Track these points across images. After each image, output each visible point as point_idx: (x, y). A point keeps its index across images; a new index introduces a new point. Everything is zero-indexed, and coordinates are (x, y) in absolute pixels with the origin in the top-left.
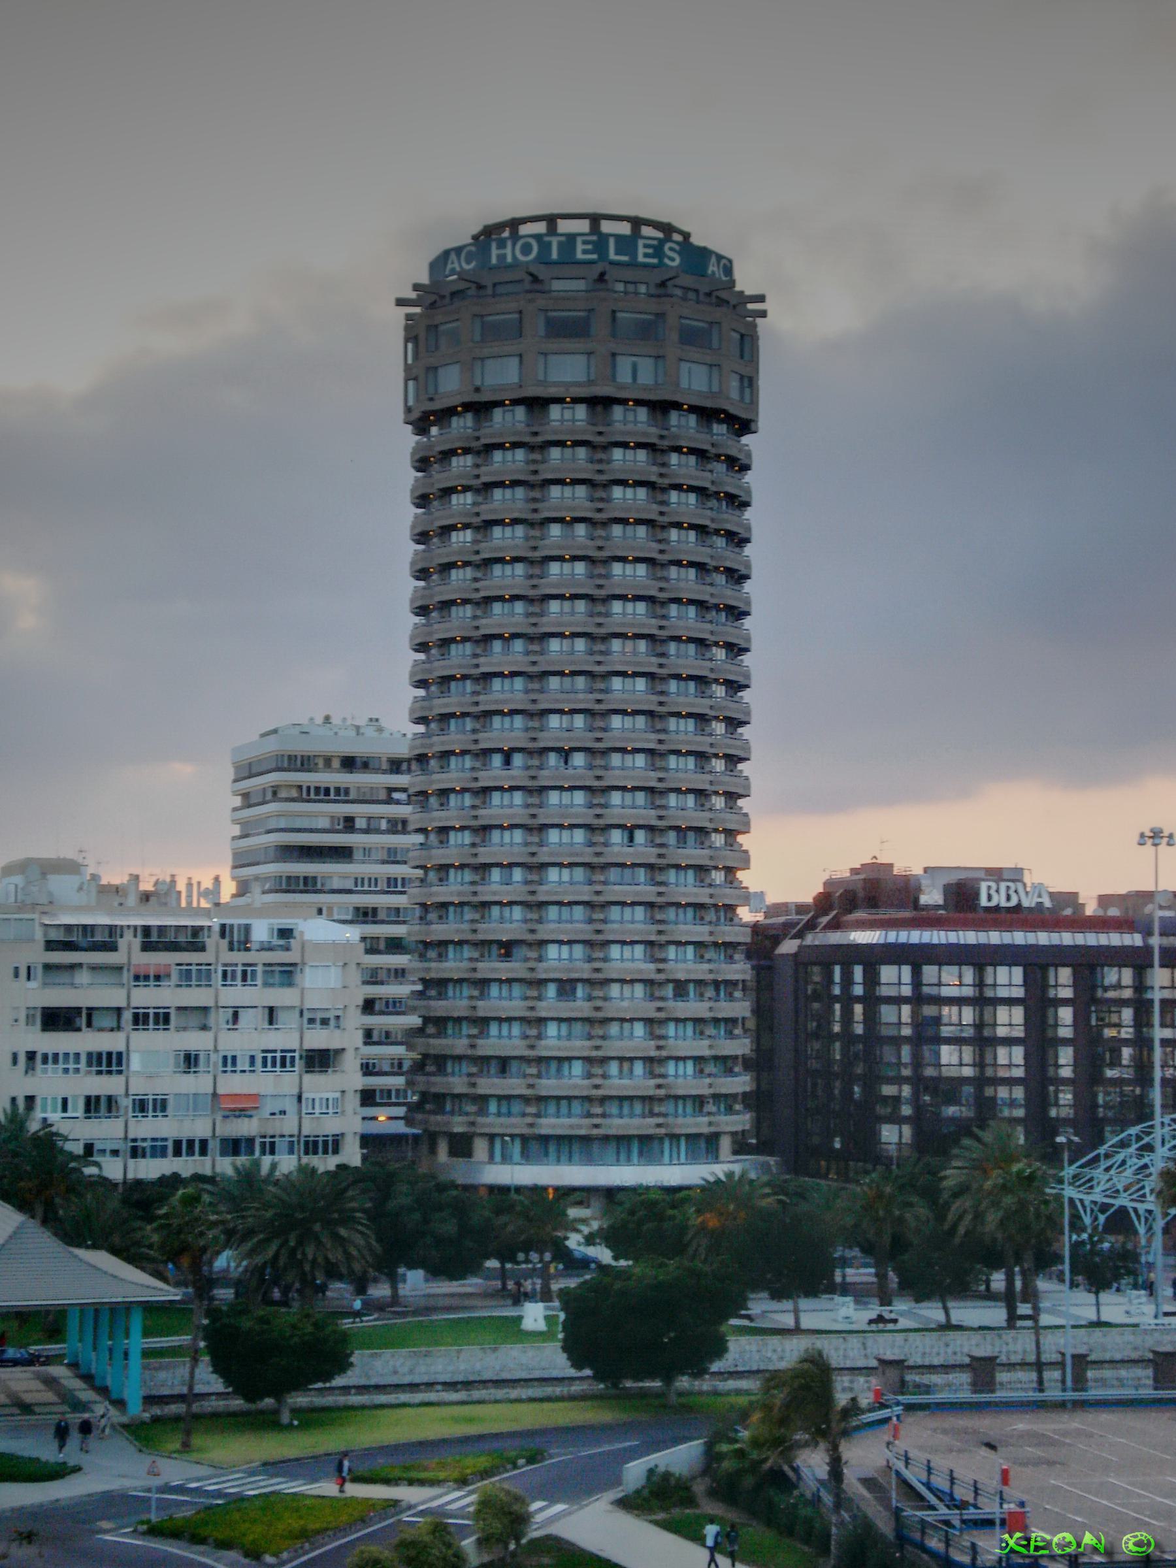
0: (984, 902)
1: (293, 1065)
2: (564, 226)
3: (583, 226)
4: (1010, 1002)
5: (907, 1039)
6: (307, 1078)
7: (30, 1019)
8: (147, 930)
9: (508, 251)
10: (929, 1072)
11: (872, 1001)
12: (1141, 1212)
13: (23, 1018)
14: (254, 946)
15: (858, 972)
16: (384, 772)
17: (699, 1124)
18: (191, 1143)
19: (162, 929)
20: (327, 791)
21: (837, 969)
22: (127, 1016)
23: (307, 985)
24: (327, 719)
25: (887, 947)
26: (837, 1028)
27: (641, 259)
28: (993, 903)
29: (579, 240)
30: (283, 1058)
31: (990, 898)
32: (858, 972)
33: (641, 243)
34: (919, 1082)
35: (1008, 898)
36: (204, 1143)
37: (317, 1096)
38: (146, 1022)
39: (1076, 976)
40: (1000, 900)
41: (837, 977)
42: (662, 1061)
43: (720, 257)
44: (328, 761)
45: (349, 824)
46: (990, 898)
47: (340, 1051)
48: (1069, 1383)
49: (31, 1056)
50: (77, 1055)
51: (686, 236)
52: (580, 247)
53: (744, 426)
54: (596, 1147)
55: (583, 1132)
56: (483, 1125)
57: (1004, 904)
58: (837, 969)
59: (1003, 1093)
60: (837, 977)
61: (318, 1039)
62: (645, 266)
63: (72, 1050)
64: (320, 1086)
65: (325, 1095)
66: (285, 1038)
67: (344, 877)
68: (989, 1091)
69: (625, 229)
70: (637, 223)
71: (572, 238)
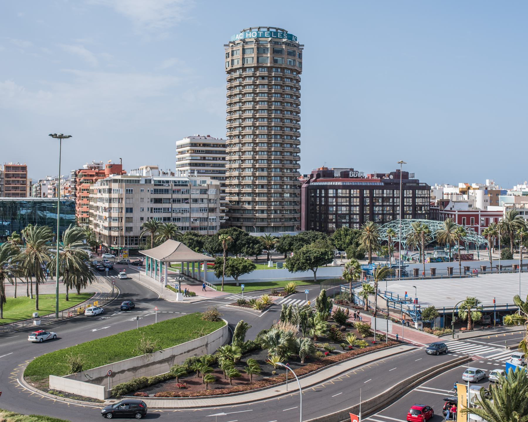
0: (350, 176)
1: (206, 211)
2: (271, 30)
3: (266, 30)
4: (356, 197)
5: (334, 205)
6: (209, 214)
7: (151, 201)
8: (175, 182)
9: (250, 35)
10: (339, 212)
11: (327, 197)
12: (404, 243)
13: (150, 201)
14: (197, 185)
15: (323, 192)
16: (212, 147)
17: (291, 224)
18: (185, 227)
19: (179, 181)
20: (200, 151)
21: (318, 191)
22: (171, 200)
23: (209, 193)
24: (199, 136)
25: (330, 186)
26: (318, 203)
27: (279, 37)
28: (352, 176)
29: (266, 32)
30: (204, 210)
31: (351, 175)
32: (323, 192)
33: (279, 33)
34: (336, 214)
35: (355, 175)
36: (188, 227)
37: (212, 218)
38: (176, 202)
39: (370, 192)
40: (353, 175)
41: (318, 192)
42: (283, 210)
43: (295, 37)
44: (200, 145)
45: (204, 158)
46: (351, 175)
47: (216, 208)
48: (144, 270)
49: (152, 208)
50: (161, 208)
51: (287, 32)
52: (266, 34)
53: (299, 73)
54: (269, 229)
55: (266, 226)
56: (245, 224)
57: (354, 176)
58: (318, 191)
59: (355, 217)
60: (318, 192)
61: (212, 206)
62: (279, 38)
63: (160, 207)
64: (212, 216)
65: (213, 217)
66: (204, 205)
67: (203, 170)
68: (352, 216)
69: (275, 30)
70: (277, 29)
71: (264, 32)
